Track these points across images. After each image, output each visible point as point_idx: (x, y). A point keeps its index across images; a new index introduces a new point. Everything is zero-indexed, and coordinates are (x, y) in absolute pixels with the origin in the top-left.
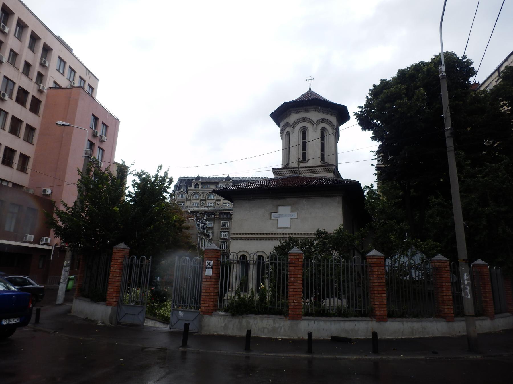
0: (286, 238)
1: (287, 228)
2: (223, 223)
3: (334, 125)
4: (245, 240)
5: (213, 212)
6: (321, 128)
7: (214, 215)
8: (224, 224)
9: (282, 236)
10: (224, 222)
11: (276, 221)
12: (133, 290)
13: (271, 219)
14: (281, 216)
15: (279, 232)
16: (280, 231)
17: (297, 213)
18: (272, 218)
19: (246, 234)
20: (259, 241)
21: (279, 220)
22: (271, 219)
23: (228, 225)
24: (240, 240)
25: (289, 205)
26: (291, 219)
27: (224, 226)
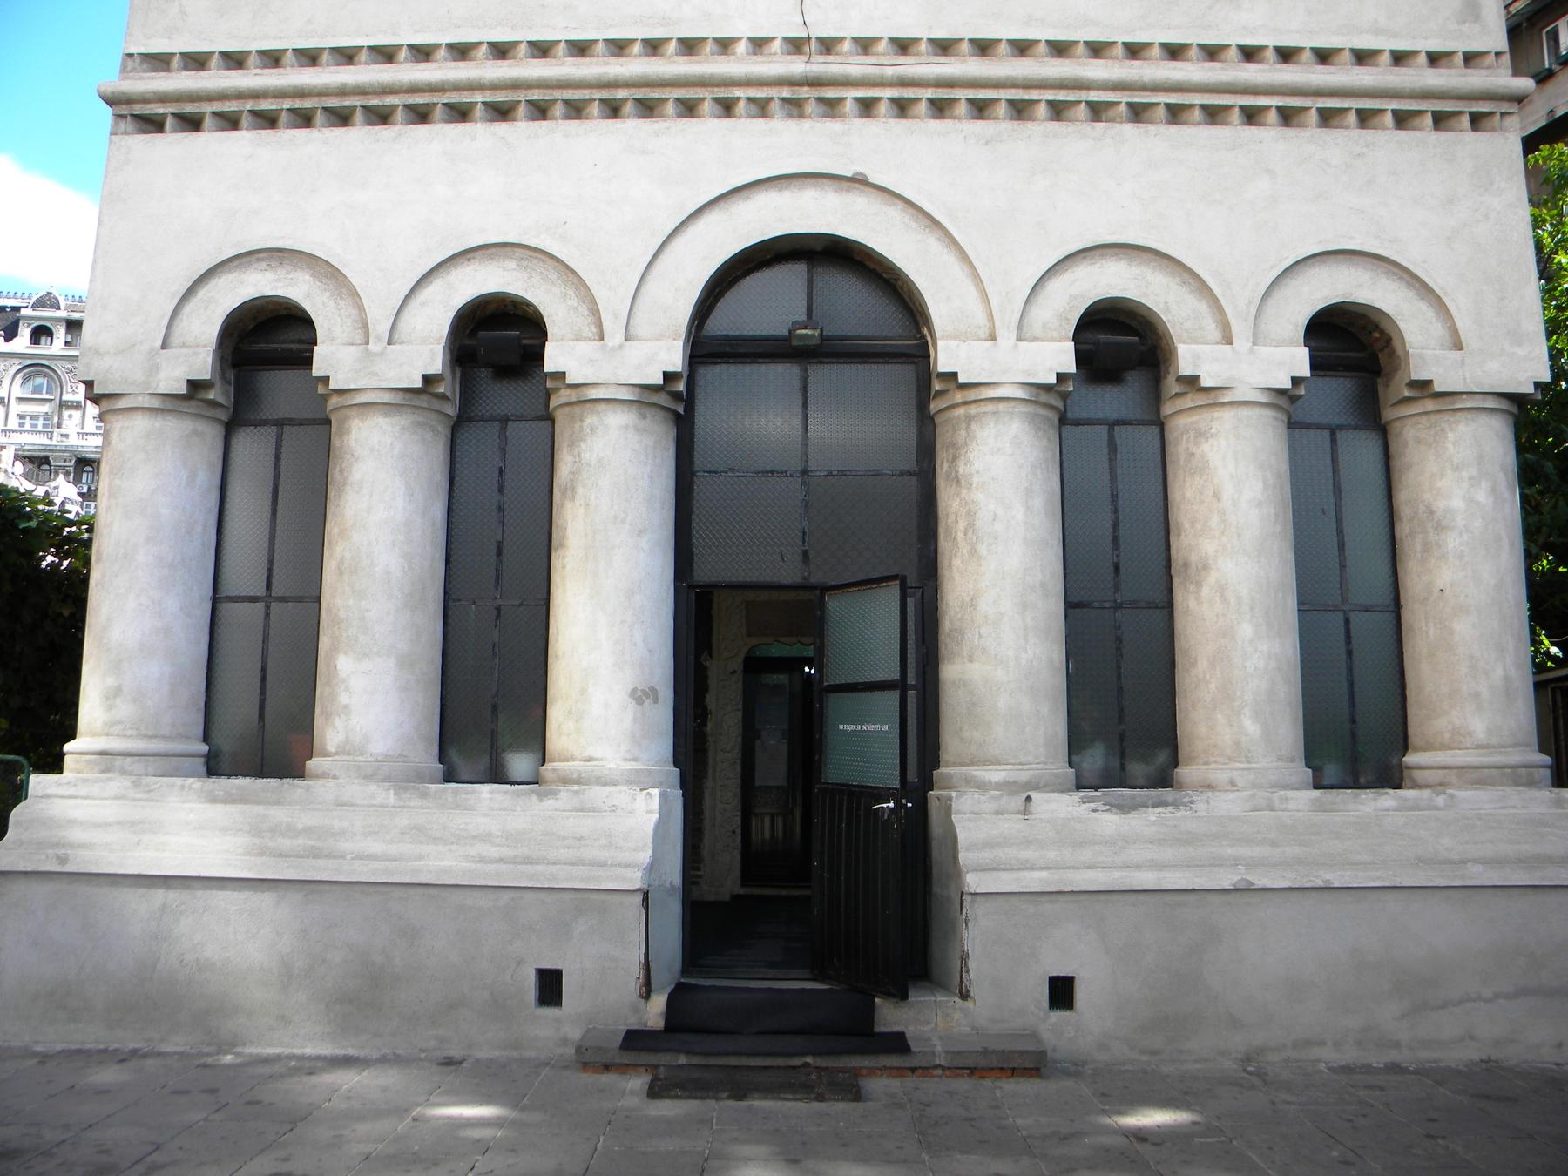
0: (830, 93)
4: (304, 119)
9: (797, 66)
20: (481, 134)
24: (230, 122)
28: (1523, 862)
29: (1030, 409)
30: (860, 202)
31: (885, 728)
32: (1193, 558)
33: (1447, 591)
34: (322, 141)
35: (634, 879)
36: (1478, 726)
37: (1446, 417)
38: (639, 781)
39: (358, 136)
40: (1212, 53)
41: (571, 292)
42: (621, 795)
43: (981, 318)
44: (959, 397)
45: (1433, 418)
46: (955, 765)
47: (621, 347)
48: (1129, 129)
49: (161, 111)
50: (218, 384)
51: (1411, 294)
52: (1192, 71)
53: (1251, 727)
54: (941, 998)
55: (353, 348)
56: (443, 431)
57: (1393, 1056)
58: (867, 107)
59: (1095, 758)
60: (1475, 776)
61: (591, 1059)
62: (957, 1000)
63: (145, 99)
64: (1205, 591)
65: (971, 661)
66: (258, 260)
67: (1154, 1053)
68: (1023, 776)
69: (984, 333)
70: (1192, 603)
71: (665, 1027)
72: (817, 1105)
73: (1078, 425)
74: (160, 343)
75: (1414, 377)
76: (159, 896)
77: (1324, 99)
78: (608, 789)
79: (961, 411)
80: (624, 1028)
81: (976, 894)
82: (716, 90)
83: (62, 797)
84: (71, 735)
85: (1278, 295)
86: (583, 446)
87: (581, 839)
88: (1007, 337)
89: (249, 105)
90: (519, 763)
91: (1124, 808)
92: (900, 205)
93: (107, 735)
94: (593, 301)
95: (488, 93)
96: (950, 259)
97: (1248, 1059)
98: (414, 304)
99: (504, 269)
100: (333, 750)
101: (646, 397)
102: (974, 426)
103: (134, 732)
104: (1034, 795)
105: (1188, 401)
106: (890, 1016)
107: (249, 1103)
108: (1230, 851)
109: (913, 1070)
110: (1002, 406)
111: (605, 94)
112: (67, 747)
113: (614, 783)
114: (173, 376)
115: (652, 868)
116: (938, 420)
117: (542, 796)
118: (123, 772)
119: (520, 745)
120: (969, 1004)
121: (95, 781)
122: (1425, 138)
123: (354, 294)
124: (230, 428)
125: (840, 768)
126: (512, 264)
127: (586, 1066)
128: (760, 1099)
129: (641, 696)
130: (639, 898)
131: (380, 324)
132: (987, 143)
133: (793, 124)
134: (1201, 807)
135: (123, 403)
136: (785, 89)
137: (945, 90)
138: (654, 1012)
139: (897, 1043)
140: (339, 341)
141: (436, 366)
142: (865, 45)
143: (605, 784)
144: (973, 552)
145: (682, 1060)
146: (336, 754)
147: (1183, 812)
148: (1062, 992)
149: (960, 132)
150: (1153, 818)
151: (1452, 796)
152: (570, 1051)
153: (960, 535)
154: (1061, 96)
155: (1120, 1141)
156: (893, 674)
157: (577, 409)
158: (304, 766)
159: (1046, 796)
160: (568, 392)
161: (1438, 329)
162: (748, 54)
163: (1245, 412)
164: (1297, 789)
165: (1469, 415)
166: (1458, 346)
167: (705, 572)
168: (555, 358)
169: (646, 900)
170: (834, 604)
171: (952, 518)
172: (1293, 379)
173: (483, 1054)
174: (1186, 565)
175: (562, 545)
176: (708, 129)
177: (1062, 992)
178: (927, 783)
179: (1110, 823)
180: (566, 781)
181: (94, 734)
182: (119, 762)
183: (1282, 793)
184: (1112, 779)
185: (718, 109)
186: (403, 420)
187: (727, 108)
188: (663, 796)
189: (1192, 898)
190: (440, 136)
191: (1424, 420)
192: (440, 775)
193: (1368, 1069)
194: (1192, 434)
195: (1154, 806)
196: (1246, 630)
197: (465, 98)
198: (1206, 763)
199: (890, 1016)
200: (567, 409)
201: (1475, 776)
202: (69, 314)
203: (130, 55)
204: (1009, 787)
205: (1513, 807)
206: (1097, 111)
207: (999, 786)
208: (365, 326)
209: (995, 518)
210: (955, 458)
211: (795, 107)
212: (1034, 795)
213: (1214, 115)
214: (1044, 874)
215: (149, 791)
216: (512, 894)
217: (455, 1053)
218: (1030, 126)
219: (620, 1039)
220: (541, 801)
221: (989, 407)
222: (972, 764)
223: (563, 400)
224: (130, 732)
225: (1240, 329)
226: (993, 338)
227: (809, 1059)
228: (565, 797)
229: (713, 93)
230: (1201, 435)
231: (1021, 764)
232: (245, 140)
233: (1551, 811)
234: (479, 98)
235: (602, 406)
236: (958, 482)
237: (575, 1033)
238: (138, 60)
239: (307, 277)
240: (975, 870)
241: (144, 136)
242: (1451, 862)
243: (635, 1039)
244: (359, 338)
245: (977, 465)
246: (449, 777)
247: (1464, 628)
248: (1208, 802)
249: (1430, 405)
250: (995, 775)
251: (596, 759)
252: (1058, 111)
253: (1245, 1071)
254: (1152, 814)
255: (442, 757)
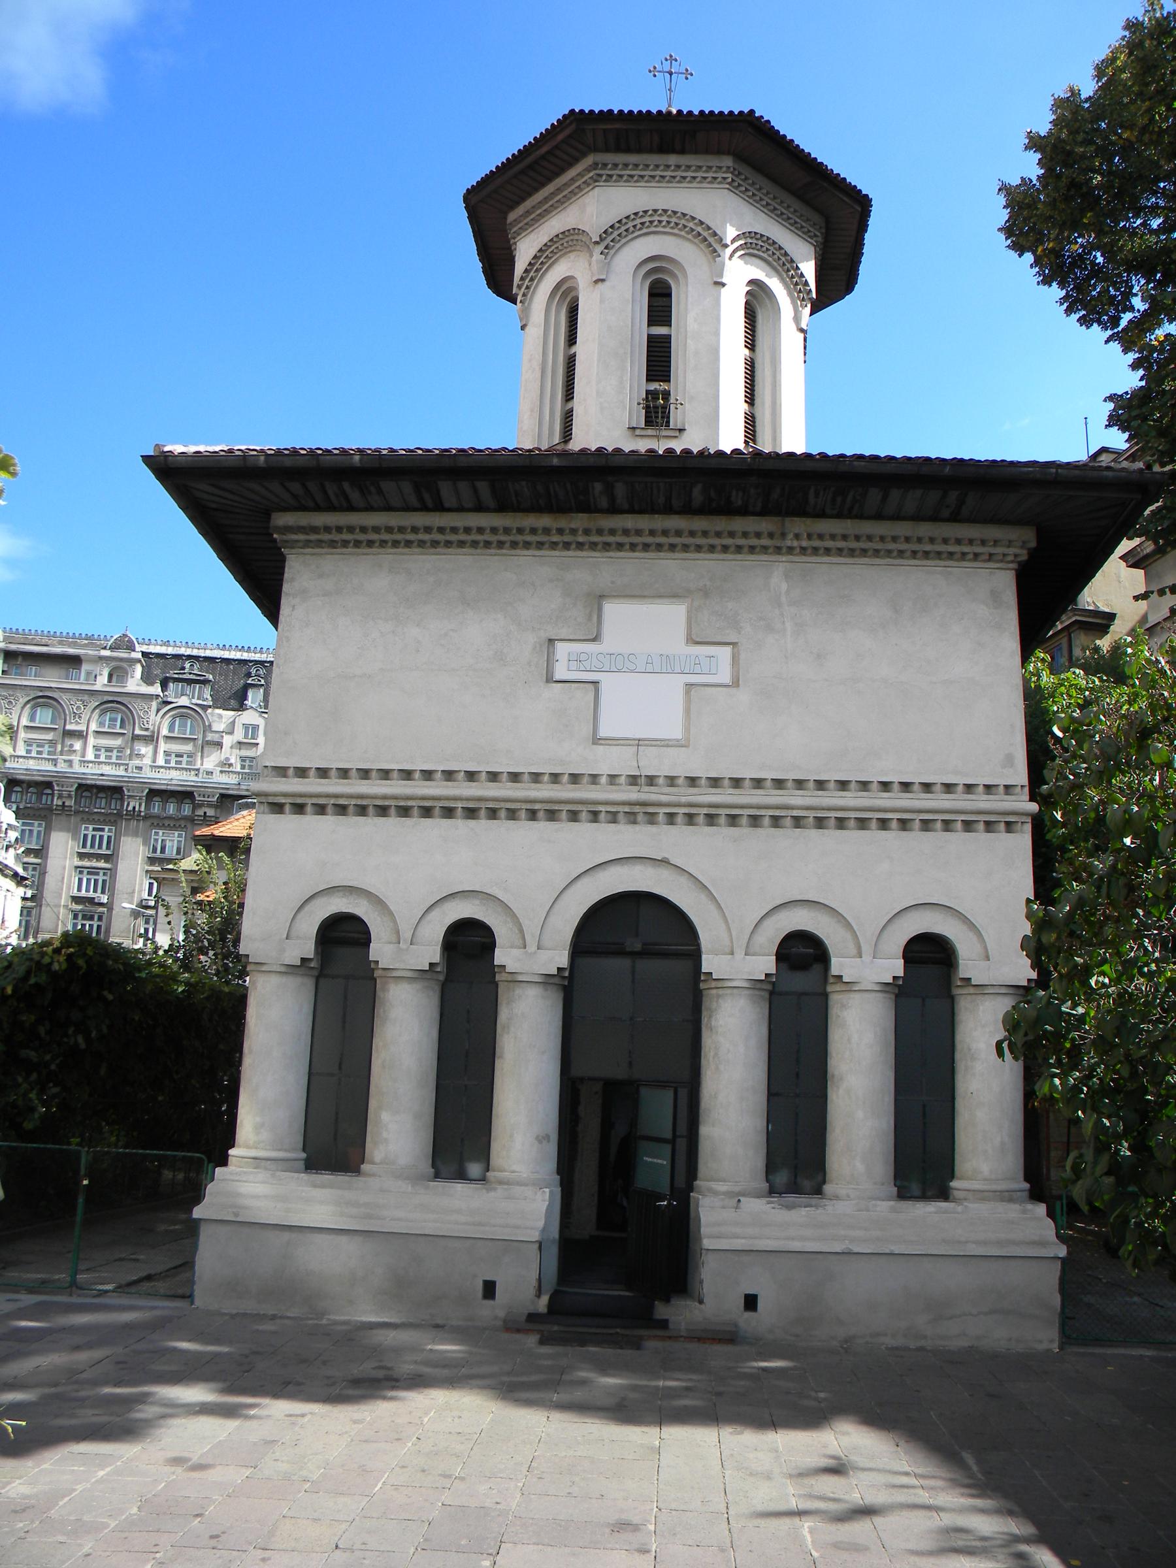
0: (651, 810)
1: (665, 743)
2: (90, 833)
3: (802, 275)
4: (362, 811)
5: (49, 785)
6: (571, 439)
7: (53, 795)
8: (94, 837)
9: (633, 794)
10: (94, 829)
11: (584, 697)
12: (1058, 740)
13: (550, 679)
14: (622, 664)
15: (604, 769)
16: (607, 761)
17: (728, 650)
18: (557, 677)
19: (365, 774)
20: (460, 826)
21: (604, 688)
22: (550, 679)
23: (109, 842)
24: (321, 810)
25: (674, 596)
26: (689, 686)
27: (92, 846)
28: (999, 1243)
29: (751, 992)
30: (665, 873)
31: (665, 1163)
32: (836, 1073)
33: (975, 1093)
34: (371, 825)
35: (535, 1236)
36: (985, 1168)
37: (980, 997)
38: (539, 1185)
39: (392, 823)
40: (864, 785)
41: (509, 919)
42: (528, 1191)
43: (727, 942)
44: (714, 984)
45: (974, 996)
46: (704, 1180)
47: (535, 953)
48: (814, 833)
49: (284, 801)
50: (315, 960)
51: (965, 927)
52: (851, 799)
53: (860, 1167)
54: (689, 1303)
55: (392, 945)
56: (437, 988)
57: (922, 1343)
58: (671, 818)
59: (782, 1178)
60: (981, 1196)
61: (511, 1326)
62: (697, 1304)
63: (275, 795)
64: (841, 1091)
65: (713, 1126)
66: (338, 891)
67: (797, 1336)
68: (737, 1189)
69: (727, 950)
70: (834, 1097)
71: (548, 1311)
72: (620, 1351)
73: (781, 995)
74: (285, 936)
75: (961, 976)
76: (286, 1236)
77: (923, 814)
78: (523, 1188)
79: (714, 991)
80: (526, 1312)
81: (708, 1250)
82: (589, 806)
83: (233, 1181)
84: (232, 1145)
85: (890, 928)
86: (514, 1005)
87: (508, 1214)
88: (740, 954)
89: (332, 801)
90: (474, 1169)
91: (789, 1207)
92: (687, 875)
93: (256, 1148)
94: (520, 925)
95: (465, 802)
96: (712, 907)
97: (846, 1341)
98: (423, 922)
99: (473, 905)
100: (378, 1162)
101: (547, 980)
102: (720, 1000)
103: (268, 1148)
104: (742, 1199)
105: (838, 987)
106: (662, 1311)
107: (349, 1340)
108: (843, 1232)
109: (670, 1338)
110: (735, 991)
111: (529, 806)
112: (231, 1152)
113: (526, 1185)
114: (293, 956)
115: (544, 1230)
116: (705, 993)
117: (488, 1190)
118: (266, 1169)
119: (476, 1159)
120: (702, 1306)
121: (251, 1173)
122: (980, 837)
123: (391, 914)
124: (317, 980)
125: (642, 1180)
126: (477, 902)
127: (507, 1329)
128: (592, 1347)
129: (542, 1139)
130: (537, 1246)
131: (407, 934)
132: (735, 841)
133: (630, 828)
134: (830, 1209)
135: (264, 968)
136: (627, 806)
137: (714, 809)
138: (542, 1304)
139: (664, 1324)
140: (383, 940)
141: (437, 958)
142: (671, 781)
143: (521, 1185)
144: (717, 1068)
145: (556, 1328)
146: (379, 1164)
147: (820, 1211)
148: (751, 1302)
149: (722, 834)
150: (804, 1213)
151: (966, 1206)
152: (499, 1323)
153: (711, 1059)
154: (777, 813)
155: (754, 1371)
156: (668, 1135)
157: (511, 984)
158: (360, 1167)
159: (748, 1199)
160: (506, 975)
161: (978, 948)
162: (607, 784)
163: (866, 995)
164: (883, 1200)
165: (991, 996)
166: (988, 958)
167: (576, 1071)
168: (500, 957)
169: (540, 1248)
170: (644, 1092)
171: (707, 1049)
172: (894, 977)
173: (454, 1323)
174: (833, 1076)
175: (501, 1057)
176: (584, 828)
177: (751, 1302)
178: (690, 1188)
179: (782, 1215)
180: (501, 1182)
181: (248, 1147)
182: (263, 1163)
183: (874, 1202)
184: (794, 1188)
185: (590, 817)
186: (417, 986)
187: (595, 816)
188: (551, 1193)
189: (820, 1256)
190: (437, 827)
191: (969, 997)
192: (432, 1175)
193: (907, 1349)
194: (839, 1005)
195: (805, 1207)
196: (860, 1114)
197: (452, 804)
198: (837, 1184)
199: (662, 1311)
200: (506, 983)
201: (981, 1196)
202: (9, 645)
203: (266, 767)
204: (730, 1194)
205: (999, 1213)
206: (798, 822)
207: (725, 1193)
208: (398, 932)
209: (729, 1051)
210: (710, 1017)
211: (632, 818)
212: (742, 1199)
213: (862, 824)
214: (743, 1241)
215: (280, 1180)
216: (472, 1241)
217: (440, 1322)
218: (759, 831)
219: (525, 1318)
220: (488, 1193)
221: (729, 991)
222: (711, 1181)
223: (504, 979)
224: (268, 1148)
225: (867, 949)
226: (732, 953)
227: (618, 1330)
228: (500, 1191)
229: (587, 807)
230: (843, 1006)
231: (736, 1182)
232: (329, 821)
233: (1020, 1216)
234: (459, 805)
235: (524, 985)
236: (711, 1030)
237: (501, 1314)
238: (270, 769)
239: (365, 902)
240: (709, 1237)
241: (274, 815)
242: (959, 1242)
243: (533, 1317)
244: (394, 939)
245: (721, 1022)
246: (437, 1176)
247: (981, 1115)
248: (833, 1205)
249: (972, 990)
250: (722, 1187)
251: (517, 1172)
252: (776, 821)
253: (842, 1347)
254: (804, 1211)
255: (434, 1165)
